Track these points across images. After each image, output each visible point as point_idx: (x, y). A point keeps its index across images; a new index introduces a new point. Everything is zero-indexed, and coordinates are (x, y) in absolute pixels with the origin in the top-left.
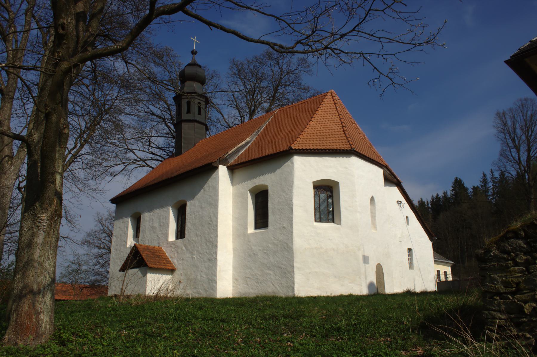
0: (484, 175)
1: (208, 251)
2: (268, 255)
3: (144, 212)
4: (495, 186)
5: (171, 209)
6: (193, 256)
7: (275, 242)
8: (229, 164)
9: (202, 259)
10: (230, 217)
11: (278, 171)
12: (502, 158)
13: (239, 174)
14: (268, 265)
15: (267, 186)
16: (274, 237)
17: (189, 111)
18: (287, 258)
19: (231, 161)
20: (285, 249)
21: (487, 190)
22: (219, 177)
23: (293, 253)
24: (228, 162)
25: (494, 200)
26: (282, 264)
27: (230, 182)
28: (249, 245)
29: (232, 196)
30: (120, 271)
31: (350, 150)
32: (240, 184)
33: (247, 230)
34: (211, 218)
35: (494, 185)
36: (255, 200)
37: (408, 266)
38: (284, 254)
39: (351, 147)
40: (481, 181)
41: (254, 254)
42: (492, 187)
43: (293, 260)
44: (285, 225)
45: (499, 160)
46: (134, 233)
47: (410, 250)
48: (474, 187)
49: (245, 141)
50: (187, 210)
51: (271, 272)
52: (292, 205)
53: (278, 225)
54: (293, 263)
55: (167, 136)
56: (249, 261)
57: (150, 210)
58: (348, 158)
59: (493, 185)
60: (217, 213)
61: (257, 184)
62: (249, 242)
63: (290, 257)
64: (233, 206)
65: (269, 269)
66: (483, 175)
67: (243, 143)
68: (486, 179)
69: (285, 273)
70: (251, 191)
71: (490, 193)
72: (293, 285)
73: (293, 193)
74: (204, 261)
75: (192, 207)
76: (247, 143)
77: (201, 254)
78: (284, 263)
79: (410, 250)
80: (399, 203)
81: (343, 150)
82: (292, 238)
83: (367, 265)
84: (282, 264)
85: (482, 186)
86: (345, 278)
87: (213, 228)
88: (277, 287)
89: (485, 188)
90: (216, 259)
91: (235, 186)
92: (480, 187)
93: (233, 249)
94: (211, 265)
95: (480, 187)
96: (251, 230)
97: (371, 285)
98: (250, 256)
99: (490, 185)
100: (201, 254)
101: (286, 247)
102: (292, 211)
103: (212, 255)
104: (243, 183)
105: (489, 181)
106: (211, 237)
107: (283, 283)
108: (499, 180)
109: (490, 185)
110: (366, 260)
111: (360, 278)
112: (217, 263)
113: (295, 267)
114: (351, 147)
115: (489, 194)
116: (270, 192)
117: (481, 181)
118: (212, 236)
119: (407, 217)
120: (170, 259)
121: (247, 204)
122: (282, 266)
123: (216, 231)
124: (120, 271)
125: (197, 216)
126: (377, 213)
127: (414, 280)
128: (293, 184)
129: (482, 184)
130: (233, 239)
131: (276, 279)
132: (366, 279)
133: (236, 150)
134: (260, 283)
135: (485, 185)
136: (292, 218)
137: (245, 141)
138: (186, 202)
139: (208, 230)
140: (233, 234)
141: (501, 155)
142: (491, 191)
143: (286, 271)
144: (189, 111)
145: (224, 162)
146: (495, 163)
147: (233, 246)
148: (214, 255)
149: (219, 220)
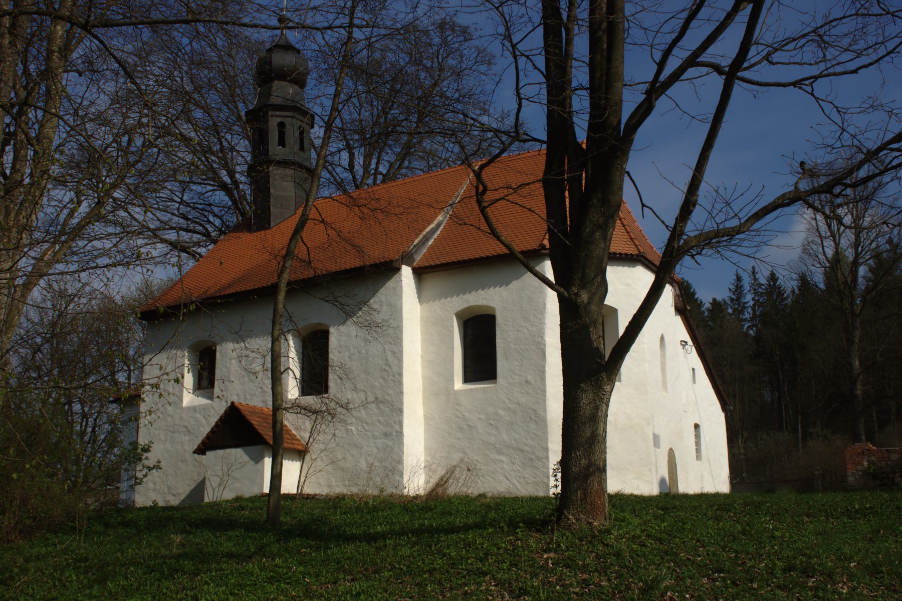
0: (739, 278)
1: (381, 419)
2: (496, 428)
3: (223, 340)
4: (758, 300)
5: (291, 338)
6: (349, 427)
7: (510, 406)
8: (415, 264)
9: (369, 433)
10: (419, 359)
11: (515, 284)
12: (806, 257)
13: (433, 283)
14: (497, 446)
15: (494, 309)
16: (508, 398)
17: (282, 142)
18: (535, 434)
19: (418, 258)
20: (531, 418)
21: (739, 311)
22: (401, 287)
23: (546, 426)
24: (414, 260)
25: (754, 329)
26: (526, 445)
27: (416, 295)
28: (457, 410)
29: (421, 321)
30: (195, 452)
31: (637, 255)
32: (437, 302)
33: (453, 384)
34: (387, 360)
35: (756, 298)
36: (462, 329)
37: (695, 455)
38: (528, 426)
39: (639, 251)
40: (730, 290)
41: (469, 426)
42: (751, 303)
43: (547, 439)
44: (530, 378)
45: (801, 259)
46: (194, 380)
47: (697, 426)
48: (714, 300)
49: (436, 222)
50: (330, 343)
51: (504, 458)
52: (544, 345)
53: (516, 377)
54: (547, 443)
55: (212, 183)
56: (459, 439)
57: (240, 336)
58: (631, 268)
59: (753, 299)
60: (401, 352)
61: (472, 304)
62: (458, 404)
63: (540, 433)
64: (423, 340)
65: (500, 452)
66: (735, 277)
67: (432, 226)
68: (741, 287)
69: (532, 459)
70: (459, 315)
71: (747, 316)
72: (546, 480)
73: (544, 323)
74: (374, 437)
75: (343, 338)
76: (438, 225)
77: (367, 423)
78: (530, 442)
79: (697, 426)
80: (684, 343)
81: (626, 254)
82: (544, 401)
83: (658, 450)
84: (526, 445)
85: (732, 300)
86: (627, 470)
87: (391, 377)
88: (516, 483)
89: (739, 305)
90: (400, 433)
91: (424, 305)
92: (729, 302)
93: (424, 415)
94: (390, 443)
95: (729, 302)
96: (458, 384)
97: (662, 482)
98: (461, 429)
99: (749, 298)
100: (367, 423)
101: (533, 417)
102: (544, 355)
103: (392, 427)
104: (443, 300)
105: (746, 291)
106: (388, 395)
107: (527, 476)
108: (766, 289)
109: (749, 298)
110: (656, 440)
111: (650, 470)
112: (403, 440)
113: (550, 449)
114: (639, 251)
115: (745, 317)
116: (499, 320)
117: (730, 290)
118: (390, 392)
119: (693, 369)
120: (294, 432)
121: (453, 337)
122: (526, 448)
123: (400, 383)
124: (195, 452)
125: (354, 354)
126: (667, 362)
127: (702, 477)
128: (545, 308)
129: (733, 297)
130: (424, 398)
131: (513, 470)
132: (657, 473)
133: (424, 237)
134: (482, 476)
135: (738, 299)
136: (544, 367)
137: (436, 222)
138: (328, 327)
139: (381, 381)
140: (424, 390)
141: (804, 251)
142: (750, 310)
143: (533, 457)
144: (282, 142)
145: (407, 259)
146: (792, 264)
147: (424, 411)
148: (397, 427)
149: (405, 365)
